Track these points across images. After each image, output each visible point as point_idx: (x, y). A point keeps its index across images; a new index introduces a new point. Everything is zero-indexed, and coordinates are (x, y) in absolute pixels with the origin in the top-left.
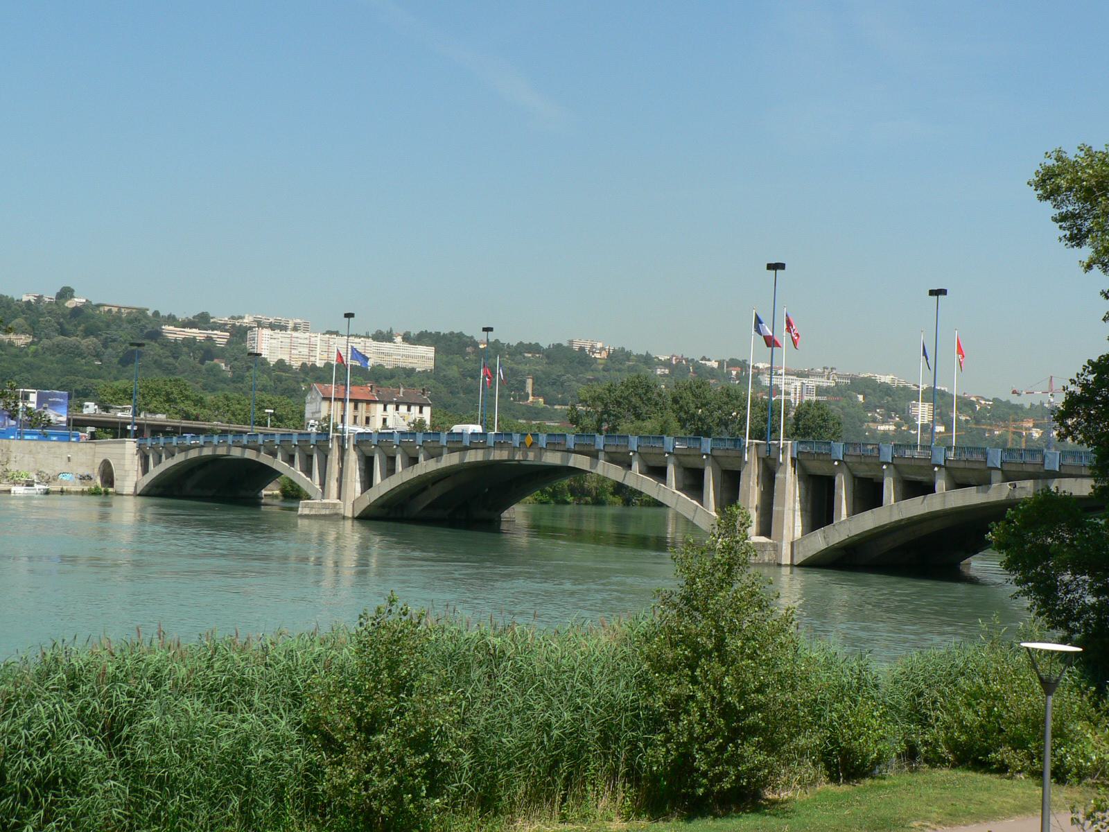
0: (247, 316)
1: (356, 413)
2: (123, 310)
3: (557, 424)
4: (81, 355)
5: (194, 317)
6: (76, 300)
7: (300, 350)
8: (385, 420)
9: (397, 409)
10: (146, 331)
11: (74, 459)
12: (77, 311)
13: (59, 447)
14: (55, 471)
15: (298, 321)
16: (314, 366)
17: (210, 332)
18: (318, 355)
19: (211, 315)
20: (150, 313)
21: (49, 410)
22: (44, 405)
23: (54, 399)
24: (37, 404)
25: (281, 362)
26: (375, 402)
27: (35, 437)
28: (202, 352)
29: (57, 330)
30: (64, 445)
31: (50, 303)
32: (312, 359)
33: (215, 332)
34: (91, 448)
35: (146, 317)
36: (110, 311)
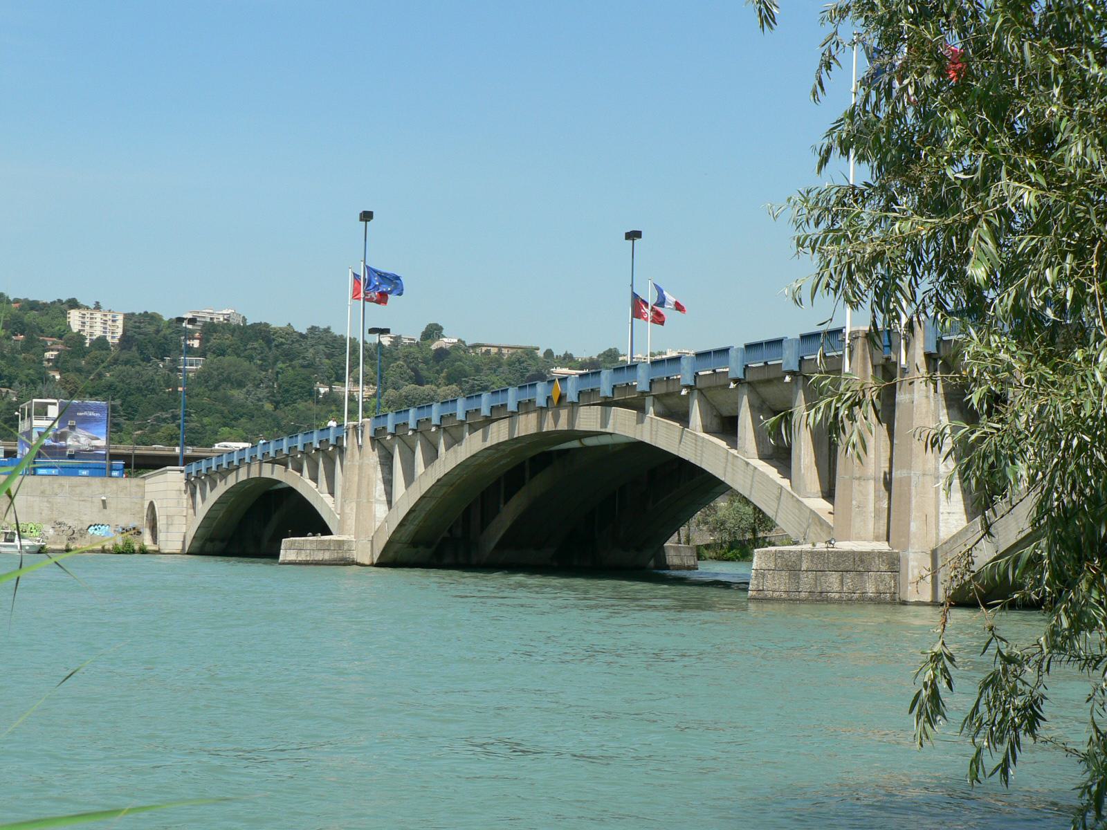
2: (505, 351)
3: (81, 414)
6: (444, 339)
10: (528, 374)
11: (112, 503)
12: (442, 353)
13: (88, 485)
14: (82, 522)
19: (621, 353)
20: (540, 353)
21: (78, 430)
23: (85, 413)
27: (53, 471)
29: (411, 378)
30: (97, 482)
31: (410, 345)
34: (138, 486)
35: (534, 358)
36: (488, 352)
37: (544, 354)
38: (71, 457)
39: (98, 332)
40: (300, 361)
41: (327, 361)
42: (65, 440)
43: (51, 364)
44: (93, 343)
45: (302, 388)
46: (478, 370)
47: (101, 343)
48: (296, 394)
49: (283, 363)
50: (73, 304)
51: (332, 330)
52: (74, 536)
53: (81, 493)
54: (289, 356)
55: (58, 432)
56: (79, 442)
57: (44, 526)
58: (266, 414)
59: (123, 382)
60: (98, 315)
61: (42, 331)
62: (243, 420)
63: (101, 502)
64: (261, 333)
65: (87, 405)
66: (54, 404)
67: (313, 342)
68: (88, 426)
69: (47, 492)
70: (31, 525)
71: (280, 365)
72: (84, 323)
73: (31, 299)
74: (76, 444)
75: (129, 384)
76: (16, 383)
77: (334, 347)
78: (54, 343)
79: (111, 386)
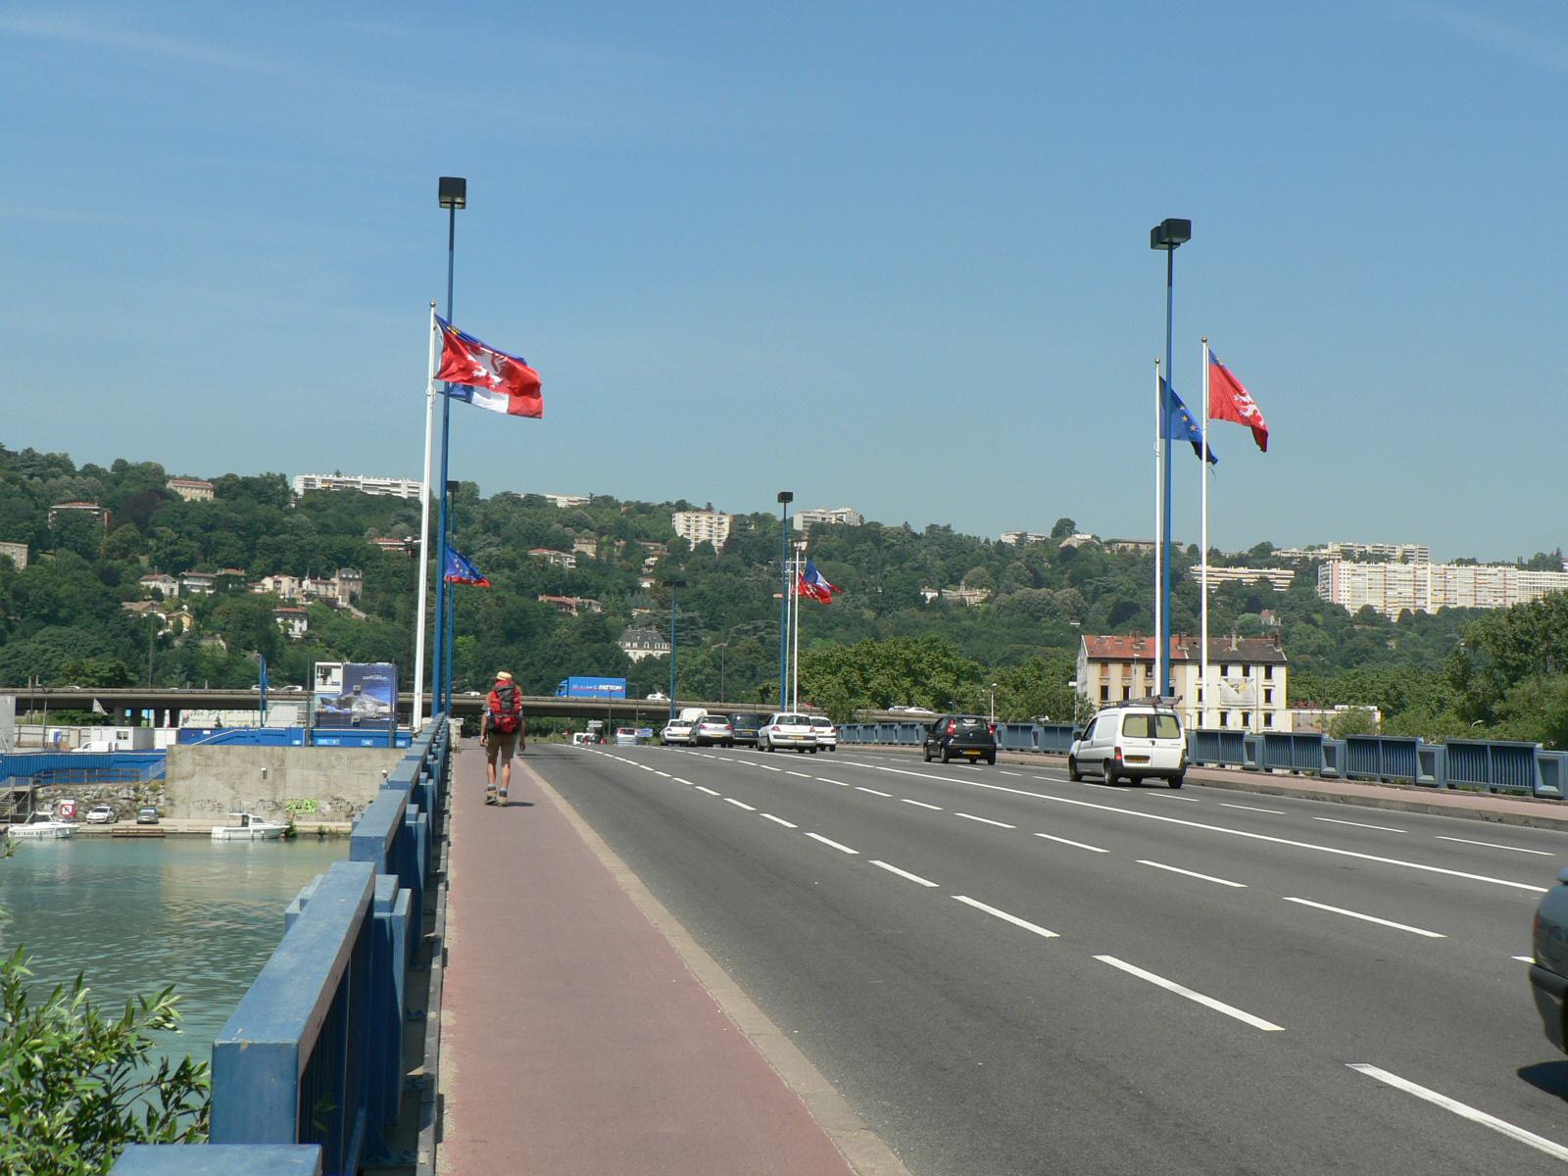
0: (1330, 544)
1: (1149, 683)
2: (1142, 547)
3: (367, 678)
4: (1053, 614)
5: (1251, 551)
6: (1078, 536)
7: (1399, 590)
8: (1126, 690)
9: (1224, 672)
13: (368, 757)
14: (361, 798)
15: (1410, 547)
16: (1421, 614)
17: (1265, 570)
18: (1429, 596)
19: (1275, 547)
21: (363, 695)
22: (356, 687)
23: (371, 677)
24: (344, 687)
25: (1367, 612)
26: (1183, 662)
27: (335, 742)
28: (1246, 600)
29: (1030, 580)
32: (1420, 603)
33: (1274, 570)
37: (1188, 550)
38: (356, 725)
39: (704, 536)
40: (911, 564)
41: (941, 562)
42: (350, 707)
43: (651, 570)
44: (697, 546)
45: (908, 593)
46: (1105, 571)
47: (706, 546)
48: (901, 600)
49: (892, 565)
50: (682, 507)
51: (952, 528)
52: (353, 813)
53: (361, 766)
54: (900, 558)
55: (343, 698)
56: (364, 708)
57: (320, 802)
58: (863, 623)
59: (715, 589)
60: (704, 518)
61: (647, 536)
62: (838, 629)
63: (382, 776)
64: (870, 533)
65: (373, 669)
66: (339, 667)
67: (927, 543)
68: (375, 691)
69: (324, 765)
70: (307, 801)
71: (888, 568)
72: (689, 526)
73: (643, 502)
74: (363, 710)
75: (721, 592)
76: (603, 594)
77: (949, 548)
78: (656, 549)
79: (701, 594)
